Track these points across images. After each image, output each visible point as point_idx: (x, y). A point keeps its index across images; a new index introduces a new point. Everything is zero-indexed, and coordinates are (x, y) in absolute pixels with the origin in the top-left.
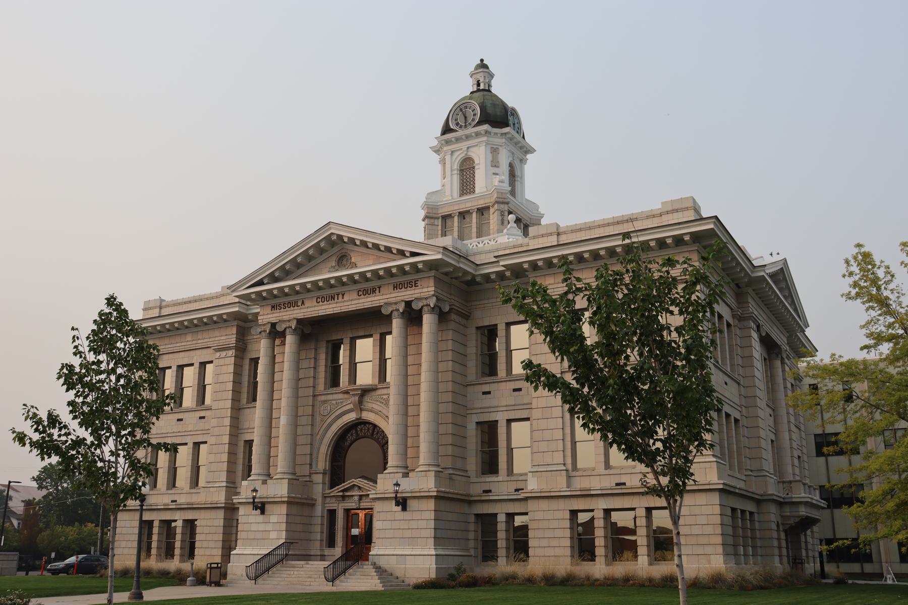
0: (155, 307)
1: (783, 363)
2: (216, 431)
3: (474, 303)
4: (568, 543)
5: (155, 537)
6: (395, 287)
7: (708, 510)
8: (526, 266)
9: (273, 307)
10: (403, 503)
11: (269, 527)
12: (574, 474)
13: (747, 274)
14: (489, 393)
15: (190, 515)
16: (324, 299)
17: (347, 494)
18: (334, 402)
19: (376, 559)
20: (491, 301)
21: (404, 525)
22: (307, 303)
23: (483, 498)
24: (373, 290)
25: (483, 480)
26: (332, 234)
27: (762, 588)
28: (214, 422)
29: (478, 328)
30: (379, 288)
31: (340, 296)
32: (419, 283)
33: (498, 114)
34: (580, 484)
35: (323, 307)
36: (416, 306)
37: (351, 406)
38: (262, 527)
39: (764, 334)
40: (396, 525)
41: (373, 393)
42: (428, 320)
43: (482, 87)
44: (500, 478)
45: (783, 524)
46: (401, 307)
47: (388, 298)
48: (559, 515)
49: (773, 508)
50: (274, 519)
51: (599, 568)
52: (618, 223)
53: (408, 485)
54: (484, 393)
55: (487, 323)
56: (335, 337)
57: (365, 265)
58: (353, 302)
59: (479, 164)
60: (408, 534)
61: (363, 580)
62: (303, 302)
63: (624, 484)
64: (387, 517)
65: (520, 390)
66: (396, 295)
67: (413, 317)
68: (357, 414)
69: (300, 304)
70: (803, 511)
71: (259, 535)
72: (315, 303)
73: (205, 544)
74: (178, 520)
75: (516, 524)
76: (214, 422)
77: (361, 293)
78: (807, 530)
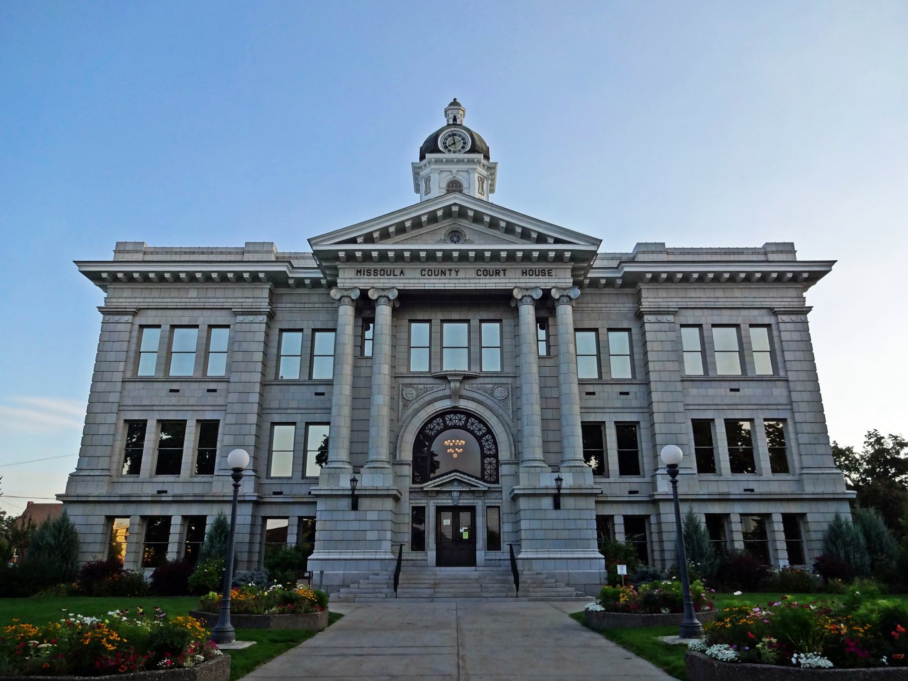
6: (524, 273)
9: (359, 272)
11: (367, 525)
14: (593, 394)
16: (486, 273)
18: (421, 386)
22: (408, 274)
24: (497, 273)
30: (504, 270)
31: (502, 272)
32: (553, 273)
35: (431, 281)
38: (355, 526)
41: (474, 381)
42: (384, 312)
44: (611, 479)
46: (355, 295)
54: (588, 393)
57: (477, 243)
58: (471, 281)
60: (565, 534)
62: (402, 272)
63: (752, 490)
65: (627, 393)
66: (527, 281)
71: (351, 536)
72: (474, 275)
75: (268, 528)
77: (479, 273)
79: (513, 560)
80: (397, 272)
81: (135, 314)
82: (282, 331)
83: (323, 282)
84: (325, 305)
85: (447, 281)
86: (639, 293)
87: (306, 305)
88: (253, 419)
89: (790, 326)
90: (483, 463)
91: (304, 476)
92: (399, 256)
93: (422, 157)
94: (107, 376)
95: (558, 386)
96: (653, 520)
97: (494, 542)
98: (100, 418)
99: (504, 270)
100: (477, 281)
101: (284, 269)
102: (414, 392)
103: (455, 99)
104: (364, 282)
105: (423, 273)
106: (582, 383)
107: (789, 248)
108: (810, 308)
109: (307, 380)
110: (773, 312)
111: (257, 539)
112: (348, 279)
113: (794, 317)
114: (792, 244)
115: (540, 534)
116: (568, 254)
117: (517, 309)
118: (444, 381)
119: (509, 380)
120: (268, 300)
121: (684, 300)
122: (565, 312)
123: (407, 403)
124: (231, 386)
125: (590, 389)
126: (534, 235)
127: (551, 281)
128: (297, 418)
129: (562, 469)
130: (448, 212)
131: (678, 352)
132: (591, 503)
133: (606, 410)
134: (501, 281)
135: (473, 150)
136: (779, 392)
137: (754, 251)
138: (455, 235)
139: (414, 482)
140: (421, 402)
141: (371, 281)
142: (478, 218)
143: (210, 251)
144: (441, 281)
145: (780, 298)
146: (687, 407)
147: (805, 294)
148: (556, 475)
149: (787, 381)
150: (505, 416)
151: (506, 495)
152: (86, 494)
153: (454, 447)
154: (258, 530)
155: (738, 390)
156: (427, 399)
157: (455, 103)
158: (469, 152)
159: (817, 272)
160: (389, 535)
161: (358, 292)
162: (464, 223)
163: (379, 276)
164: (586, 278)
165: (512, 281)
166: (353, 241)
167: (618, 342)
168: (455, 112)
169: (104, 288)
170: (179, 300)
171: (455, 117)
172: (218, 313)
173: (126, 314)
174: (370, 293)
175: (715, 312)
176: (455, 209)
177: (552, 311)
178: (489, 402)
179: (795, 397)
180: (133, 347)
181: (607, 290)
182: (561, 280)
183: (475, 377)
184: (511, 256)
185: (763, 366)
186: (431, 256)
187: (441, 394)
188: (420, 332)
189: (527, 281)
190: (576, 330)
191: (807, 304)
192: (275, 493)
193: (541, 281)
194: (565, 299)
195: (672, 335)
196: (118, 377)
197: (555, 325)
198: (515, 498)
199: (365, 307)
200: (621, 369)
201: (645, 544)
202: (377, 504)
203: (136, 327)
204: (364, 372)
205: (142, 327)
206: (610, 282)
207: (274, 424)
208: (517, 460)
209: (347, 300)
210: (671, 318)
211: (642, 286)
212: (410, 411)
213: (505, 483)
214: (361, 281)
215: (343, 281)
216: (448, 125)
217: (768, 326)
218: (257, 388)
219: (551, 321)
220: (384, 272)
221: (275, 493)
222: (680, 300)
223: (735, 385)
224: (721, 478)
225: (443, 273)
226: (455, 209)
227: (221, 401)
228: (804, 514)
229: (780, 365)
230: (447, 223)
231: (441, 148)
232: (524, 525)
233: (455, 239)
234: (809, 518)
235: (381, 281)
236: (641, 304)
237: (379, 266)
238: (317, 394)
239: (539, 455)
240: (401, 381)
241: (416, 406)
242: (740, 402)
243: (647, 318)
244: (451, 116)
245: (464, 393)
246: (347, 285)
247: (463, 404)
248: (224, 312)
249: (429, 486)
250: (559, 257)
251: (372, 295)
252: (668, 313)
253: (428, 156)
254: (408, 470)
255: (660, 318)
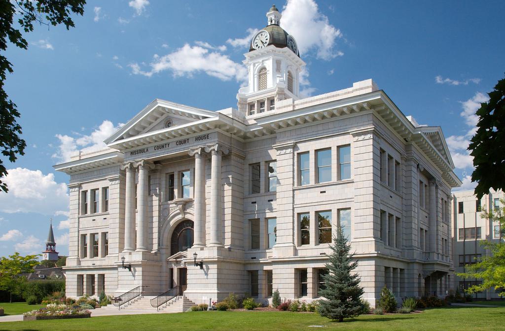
0: (77, 156)
1: (437, 187)
2: (112, 226)
3: (248, 150)
5: (85, 283)
7: (369, 268)
8: (273, 125)
13: (410, 132)
15: (101, 272)
17: (178, 260)
19: (186, 295)
23: (251, 262)
25: (251, 252)
26: (159, 106)
28: (111, 221)
29: (250, 165)
33: (281, 39)
36: (208, 150)
37: (179, 211)
39: (422, 170)
42: (214, 158)
43: (273, 23)
45: (423, 275)
46: (199, 151)
49: (416, 267)
53: (203, 255)
55: (254, 162)
56: (170, 171)
59: (268, 71)
61: (175, 306)
63: (325, 254)
64: (193, 273)
67: (206, 157)
68: (182, 215)
69: (145, 151)
70: (437, 268)
73: (109, 287)
74: (96, 273)
76: (111, 221)
77: (178, 143)
78: (442, 277)
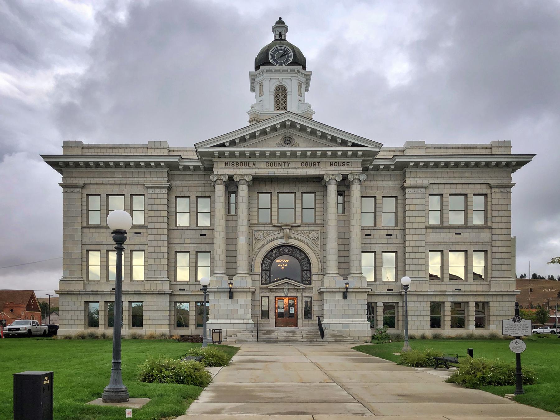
4: (83, 318)
6: (331, 164)
10: (231, 294)
12: (87, 282)
14: (370, 235)
16: (307, 164)
18: (266, 232)
20: (372, 182)
21: (346, 307)
22: (257, 165)
24: (314, 164)
27: (490, 339)
31: (317, 164)
32: (350, 164)
34: (90, 288)
35: (273, 170)
38: (231, 307)
40: (339, 307)
41: (297, 228)
42: (243, 190)
46: (225, 178)
47: (330, 171)
48: (425, 304)
50: (241, 301)
51: (447, 331)
52: (464, 148)
58: (298, 170)
60: (349, 312)
62: (254, 164)
63: (460, 290)
65: (391, 235)
66: (333, 169)
71: (229, 312)
72: (299, 166)
77: (303, 164)
79: (320, 325)
80: (251, 164)
81: (83, 187)
82: (176, 197)
83: (202, 168)
84: (203, 182)
85: (282, 170)
86: (405, 174)
87: (191, 182)
88: (165, 249)
89: (499, 195)
90: (302, 274)
91: (196, 281)
92: (253, 154)
93: (257, 68)
94: (71, 225)
95: (349, 232)
96: (400, 305)
97: (307, 314)
98: (72, 249)
99: (319, 163)
100: (302, 170)
101: (177, 160)
102: (262, 235)
103: (280, 18)
104: (230, 171)
105: (267, 164)
106: (363, 229)
107: (507, 145)
108: (515, 184)
109: (195, 227)
110: (490, 186)
111: (173, 313)
112: (221, 170)
113: (502, 190)
114: (510, 142)
115: (335, 312)
116: (360, 153)
117: (326, 186)
118: (280, 228)
119: (319, 228)
120: (167, 179)
121: (433, 179)
122: (356, 190)
123: (257, 241)
124: (149, 231)
125: (368, 232)
126: (339, 141)
127: (348, 169)
128: (190, 249)
129: (349, 279)
130: (283, 125)
131: (426, 211)
132: (365, 296)
133: (377, 245)
134: (317, 169)
135: (294, 63)
136: (486, 235)
137: (485, 147)
138: (288, 140)
139: (262, 284)
140: (266, 240)
141: (234, 170)
142: (303, 129)
143: (126, 147)
144: (279, 170)
145: (494, 178)
146: (427, 244)
147: (512, 175)
148: (345, 282)
149: (492, 228)
150: (316, 249)
151: (315, 291)
152: (72, 290)
153: (282, 263)
154: (173, 309)
155: (460, 234)
156: (270, 238)
157: (280, 22)
158: (292, 64)
159: (521, 162)
160: (250, 311)
161: (227, 177)
162: (292, 131)
163: (239, 167)
164: (371, 165)
165: (323, 169)
166: (223, 145)
167: (389, 205)
168: (280, 29)
169: (60, 171)
170: (110, 179)
171: (280, 33)
172: (136, 187)
173: (77, 188)
174: (235, 178)
175: (453, 186)
176: (288, 123)
177: (348, 187)
178: (307, 241)
179: (494, 238)
180: (85, 208)
181: (384, 172)
182: (354, 169)
183: (299, 226)
184: (324, 154)
185: (478, 220)
186: (273, 154)
187: (277, 236)
188: (264, 198)
189: (333, 169)
190: (362, 197)
191: (513, 182)
192: (180, 290)
193: (342, 169)
194: (357, 181)
195: (423, 201)
196: (79, 225)
197: (350, 195)
198: (321, 293)
199: (231, 185)
200: (388, 220)
201: (394, 317)
202: (243, 295)
203: (85, 196)
204: (232, 223)
205: (88, 195)
206: (387, 167)
207: (176, 252)
208: (323, 273)
209: (220, 182)
210: (423, 190)
211: (407, 170)
212: (259, 246)
213: (316, 285)
214: (228, 170)
215: (217, 170)
216: (276, 40)
217: (486, 195)
218: (166, 232)
219: (346, 193)
220: (242, 164)
221: (180, 290)
222: (430, 179)
223: (458, 231)
224: (443, 283)
225: (280, 164)
226: (288, 123)
227: (143, 239)
228: (488, 302)
229: (489, 219)
230: (283, 131)
231: (271, 61)
232: (326, 307)
233: (287, 142)
234: (491, 304)
235: (241, 170)
236: (405, 182)
237: (239, 160)
238: (201, 235)
239: (335, 270)
240: (253, 228)
241: (263, 243)
242: (460, 241)
243: (408, 190)
244: (278, 33)
245: (292, 235)
246: (219, 173)
247: (291, 242)
248: (139, 187)
249: (271, 286)
250: (355, 154)
251: (236, 179)
252: (422, 187)
253: (261, 67)
254: (258, 278)
255: (416, 190)
